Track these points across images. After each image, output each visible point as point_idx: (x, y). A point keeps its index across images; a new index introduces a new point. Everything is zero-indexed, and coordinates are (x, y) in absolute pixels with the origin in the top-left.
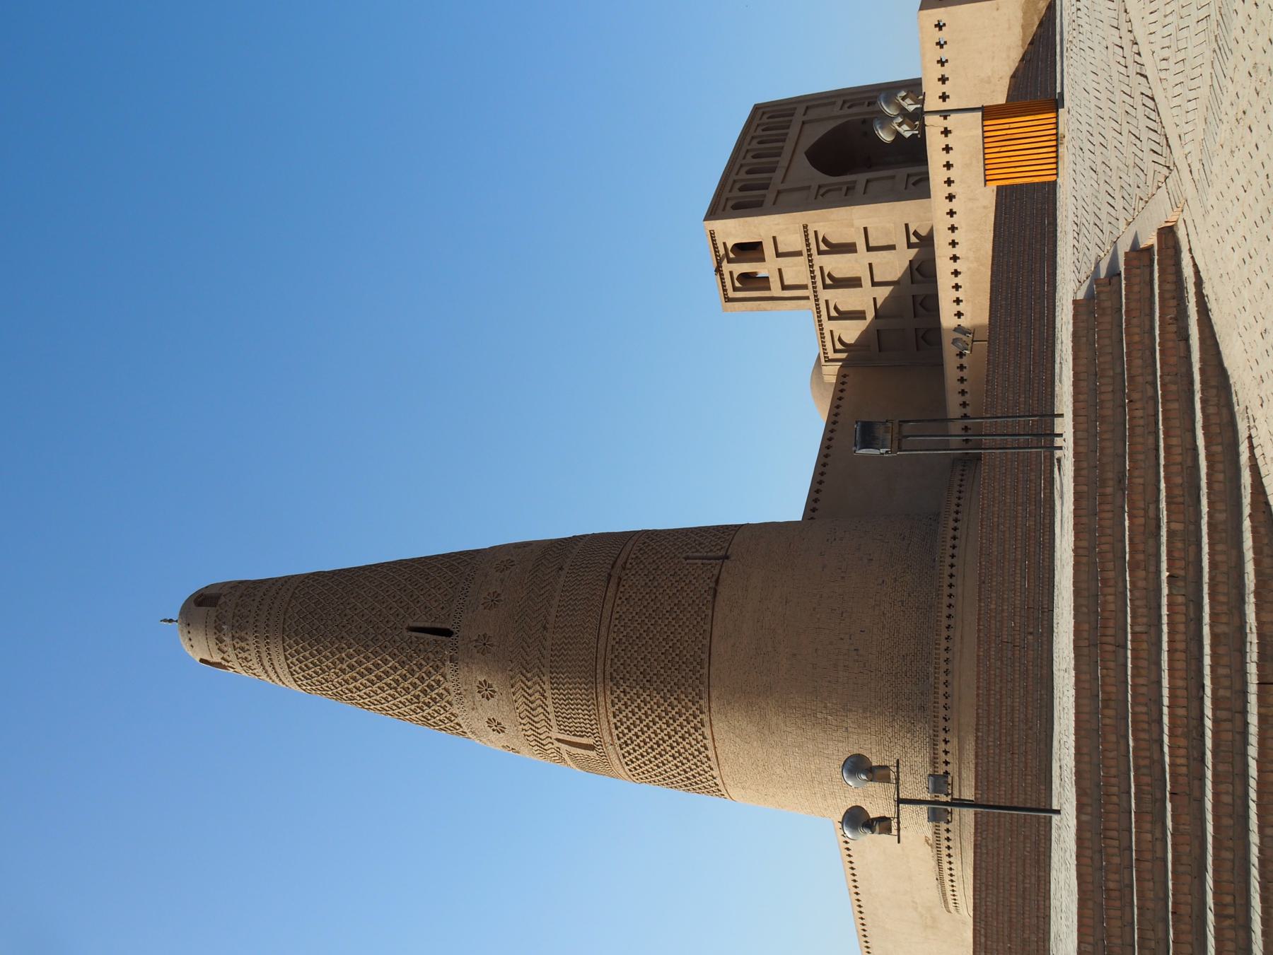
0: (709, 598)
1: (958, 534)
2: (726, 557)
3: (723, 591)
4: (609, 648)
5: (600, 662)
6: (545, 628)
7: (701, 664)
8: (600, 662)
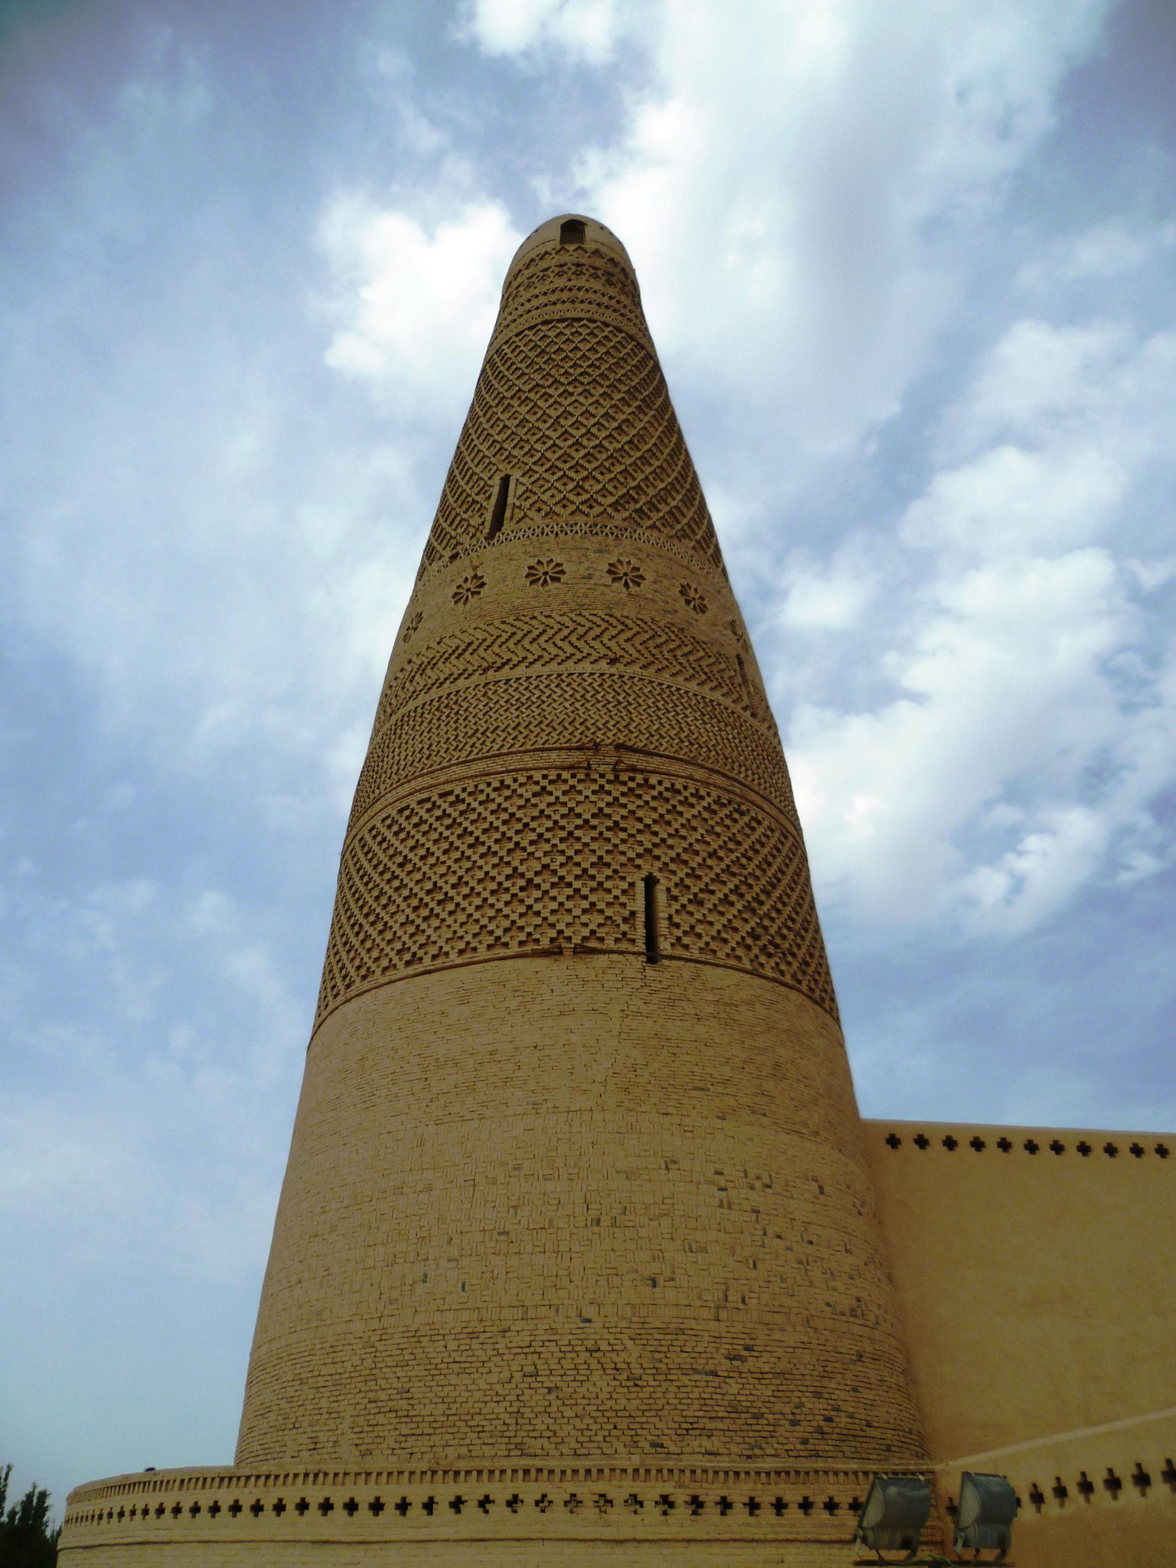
2: (652, 955)
4: (448, 788)
6: (485, 671)
7: (415, 960)
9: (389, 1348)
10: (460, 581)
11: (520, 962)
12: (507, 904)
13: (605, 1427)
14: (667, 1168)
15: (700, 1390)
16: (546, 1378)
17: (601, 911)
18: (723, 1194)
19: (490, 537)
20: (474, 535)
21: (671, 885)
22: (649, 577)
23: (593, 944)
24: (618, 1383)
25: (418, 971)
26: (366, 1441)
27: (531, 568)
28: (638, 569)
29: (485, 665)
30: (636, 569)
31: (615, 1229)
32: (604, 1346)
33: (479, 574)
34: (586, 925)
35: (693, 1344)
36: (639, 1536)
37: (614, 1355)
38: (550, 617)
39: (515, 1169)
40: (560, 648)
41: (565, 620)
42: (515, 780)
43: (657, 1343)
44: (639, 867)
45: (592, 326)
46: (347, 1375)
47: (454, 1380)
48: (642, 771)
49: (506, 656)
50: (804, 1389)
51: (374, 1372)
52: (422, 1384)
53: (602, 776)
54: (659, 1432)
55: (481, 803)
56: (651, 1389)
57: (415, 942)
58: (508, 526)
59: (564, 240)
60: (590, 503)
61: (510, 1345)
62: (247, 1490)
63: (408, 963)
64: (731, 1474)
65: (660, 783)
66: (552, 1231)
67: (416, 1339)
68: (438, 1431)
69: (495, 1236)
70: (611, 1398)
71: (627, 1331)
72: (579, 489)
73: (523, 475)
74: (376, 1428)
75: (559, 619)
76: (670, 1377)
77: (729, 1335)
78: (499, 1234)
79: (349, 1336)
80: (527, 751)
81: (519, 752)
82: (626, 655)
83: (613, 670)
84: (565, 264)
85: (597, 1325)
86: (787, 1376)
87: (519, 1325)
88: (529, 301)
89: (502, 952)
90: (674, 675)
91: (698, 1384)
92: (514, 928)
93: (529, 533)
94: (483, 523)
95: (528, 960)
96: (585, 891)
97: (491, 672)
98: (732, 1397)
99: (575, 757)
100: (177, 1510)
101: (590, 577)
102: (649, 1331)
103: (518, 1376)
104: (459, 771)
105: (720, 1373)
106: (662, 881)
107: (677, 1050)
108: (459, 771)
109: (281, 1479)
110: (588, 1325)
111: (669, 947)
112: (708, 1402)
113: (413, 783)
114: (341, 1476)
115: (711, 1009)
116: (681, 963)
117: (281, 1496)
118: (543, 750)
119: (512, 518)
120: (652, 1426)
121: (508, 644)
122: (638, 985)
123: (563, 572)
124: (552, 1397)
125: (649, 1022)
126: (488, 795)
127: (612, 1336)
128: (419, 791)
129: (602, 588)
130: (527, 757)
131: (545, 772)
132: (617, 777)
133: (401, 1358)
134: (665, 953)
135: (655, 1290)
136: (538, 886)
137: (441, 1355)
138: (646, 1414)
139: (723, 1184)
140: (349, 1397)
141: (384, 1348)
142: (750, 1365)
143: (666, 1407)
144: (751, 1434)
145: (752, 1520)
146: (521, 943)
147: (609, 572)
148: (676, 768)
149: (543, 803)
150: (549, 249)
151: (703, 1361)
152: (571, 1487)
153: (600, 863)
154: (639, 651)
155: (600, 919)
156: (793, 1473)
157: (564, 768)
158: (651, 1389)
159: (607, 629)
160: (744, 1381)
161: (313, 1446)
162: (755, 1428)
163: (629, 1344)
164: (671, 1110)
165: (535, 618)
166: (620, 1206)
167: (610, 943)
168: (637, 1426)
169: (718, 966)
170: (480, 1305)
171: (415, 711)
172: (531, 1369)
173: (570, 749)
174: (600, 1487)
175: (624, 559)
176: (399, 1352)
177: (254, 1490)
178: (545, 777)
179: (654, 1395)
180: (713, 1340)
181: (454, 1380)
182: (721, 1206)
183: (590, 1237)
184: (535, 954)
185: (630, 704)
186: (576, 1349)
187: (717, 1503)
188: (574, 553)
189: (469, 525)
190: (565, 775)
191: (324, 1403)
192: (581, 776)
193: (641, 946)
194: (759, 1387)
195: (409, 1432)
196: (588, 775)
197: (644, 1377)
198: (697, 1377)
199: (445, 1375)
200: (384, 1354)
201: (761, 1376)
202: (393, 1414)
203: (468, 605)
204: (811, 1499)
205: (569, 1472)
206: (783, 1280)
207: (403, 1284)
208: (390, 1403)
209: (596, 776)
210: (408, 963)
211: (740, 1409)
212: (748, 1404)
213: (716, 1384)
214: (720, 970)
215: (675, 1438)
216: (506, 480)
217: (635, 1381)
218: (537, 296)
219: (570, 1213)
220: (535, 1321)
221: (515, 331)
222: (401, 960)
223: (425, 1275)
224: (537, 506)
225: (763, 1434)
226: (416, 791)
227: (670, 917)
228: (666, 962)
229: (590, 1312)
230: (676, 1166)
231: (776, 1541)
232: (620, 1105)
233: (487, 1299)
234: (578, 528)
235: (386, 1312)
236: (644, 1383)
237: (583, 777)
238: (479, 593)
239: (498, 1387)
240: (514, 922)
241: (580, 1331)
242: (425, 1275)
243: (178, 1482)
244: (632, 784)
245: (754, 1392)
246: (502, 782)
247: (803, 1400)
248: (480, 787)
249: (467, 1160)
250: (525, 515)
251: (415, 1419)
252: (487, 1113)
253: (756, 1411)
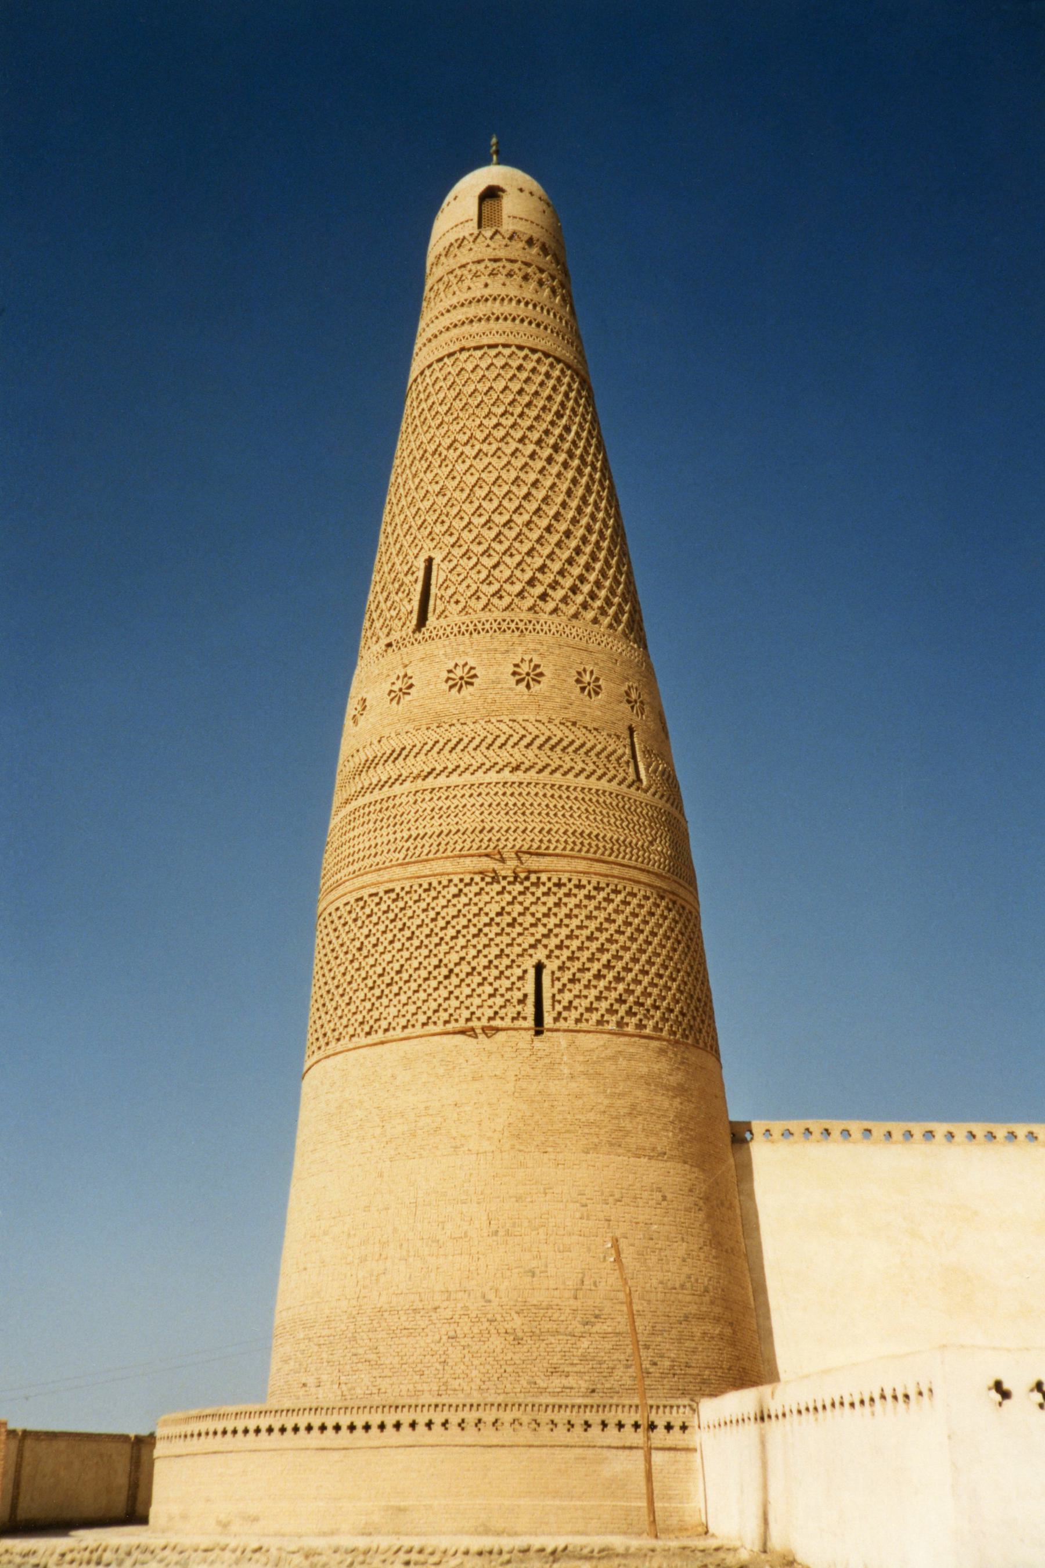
1: (596, 1430)
4: (390, 886)
18: (584, 1209)
30: (537, 666)
32: (499, 1318)
42: (440, 883)
48: (535, 872)
58: (432, 620)
65: (549, 879)
80: (448, 857)
81: (442, 858)
85: (495, 1304)
87: (446, 1304)
95: (451, 1036)
100: (235, 1432)
103: (445, 1338)
104: (398, 872)
115: (581, 1068)
118: (460, 856)
122: (529, 1053)
123: (475, 676)
124: (466, 1351)
125: (535, 1083)
128: (369, 886)
131: (462, 876)
139: (584, 1201)
142: (597, 1328)
157: (475, 873)
163: (515, 1316)
175: (527, 658)
178: (461, 880)
181: (404, 1340)
191: (325, 1356)
193: (530, 1023)
201: (604, 1335)
207: (371, 1275)
211: (589, 1358)
217: (518, 1340)
227: (554, 996)
228: (549, 1034)
229: (491, 1296)
232: (513, 1147)
239: (433, 1345)
246: (430, 884)
252: (424, 1153)
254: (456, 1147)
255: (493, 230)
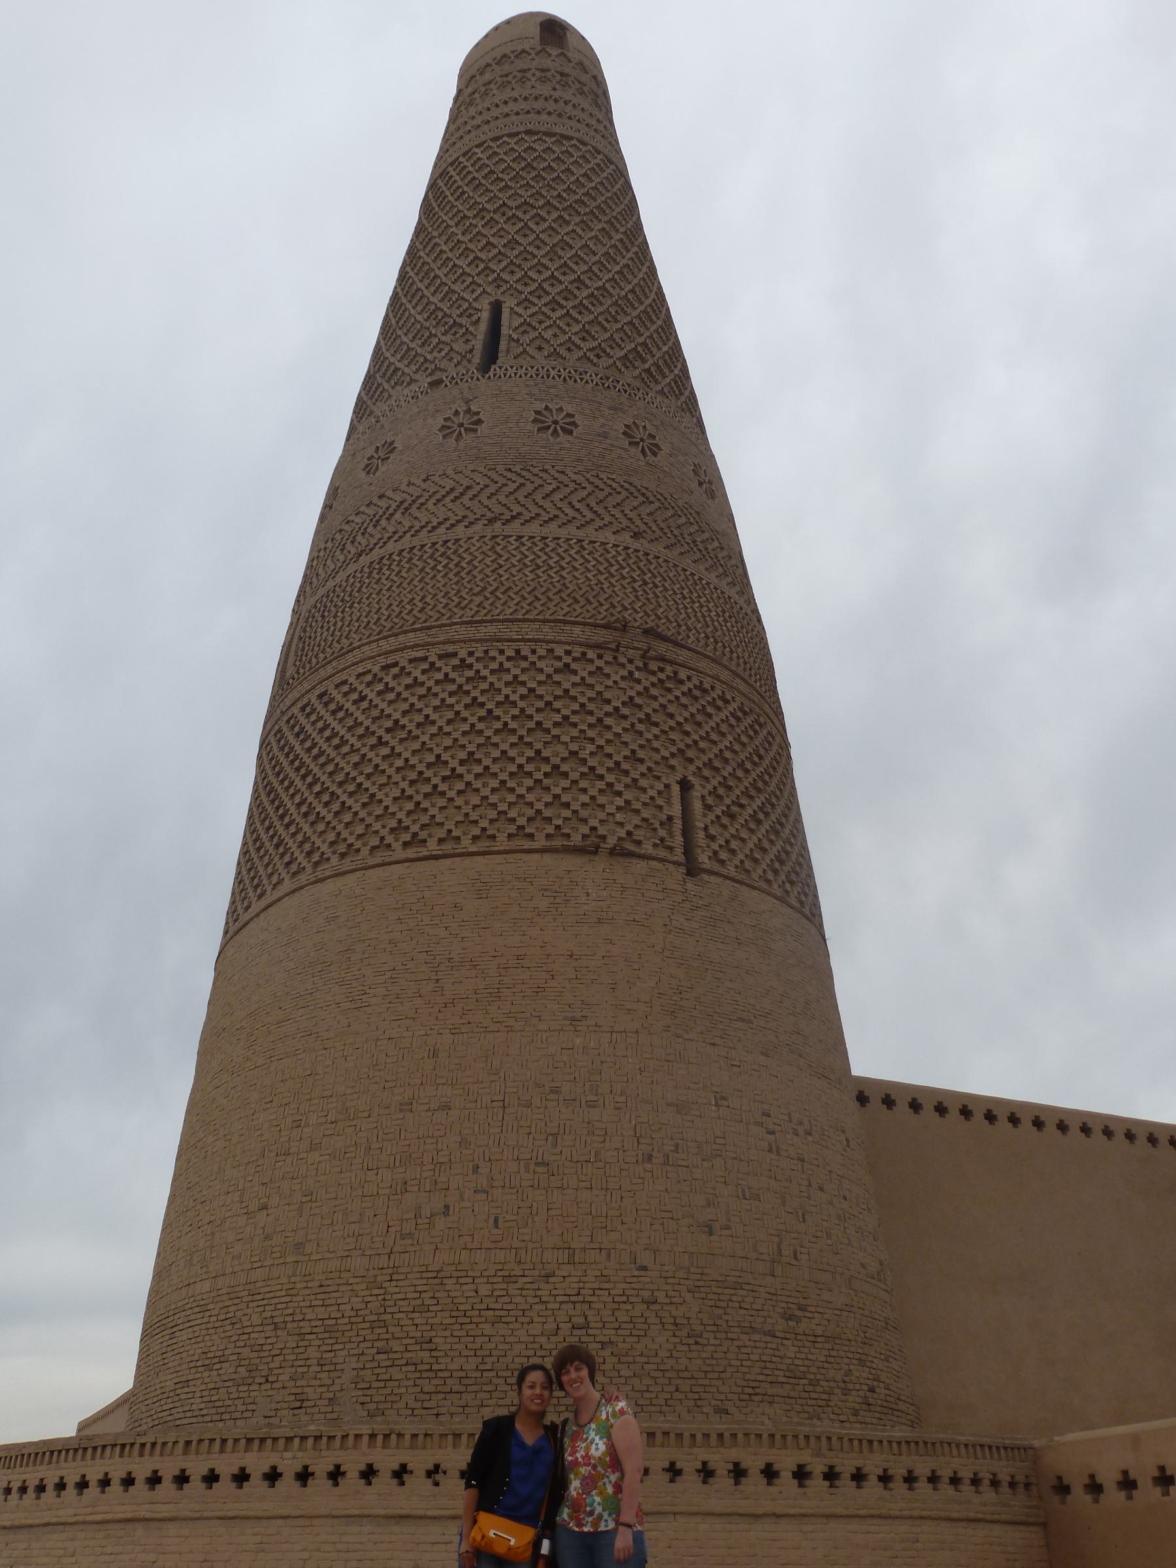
0: (576, 839)
1: (755, 1482)
2: (692, 870)
3: (592, 874)
4: (450, 648)
5: (422, 637)
6: (491, 521)
7: (415, 841)
8: (422, 637)
9: (403, 1290)
10: (449, 413)
11: (548, 859)
12: (529, 789)
13: (666, 1389)
14: (717, 1105)
15: (759, 1351)
16: (597, 1332)
17: (637, 811)
18: (772, 1137)
19: (485, 368)
20: (459, 363)
21: (706, 792)
22: (666, 448)
23: (631, 847)
24: (678, 1340)
25: (421, 855)
26: (375, 1399)
27: (537, 412)
28: (654, 437)
29: (489, 515)
30: (652, 437)
31: (669, 1168)
33: (474, 408)
34: (621, 824)
35: (752, 1300)
36: (778, 1511)
37: (672, 1308)
38: (563, 472)
39: (552, 1091)
40: (578, 510)
41: (579, 478)
42: (534, 652)
43: (716, 1297)
44: (672, 768)
45: (584, 149)
46: (346, 1320)
47: (488, 1329)
48: (671, 662)
49: (517, 509)
50: (851, 1355)
51: (383, 1317)
52: (447, 1333)
53: (631, 661)
54: (722, 1397)
55: (493, 672)
56: (713, 1348)
57: (414, 821)
59: (543, 41)
60: (599, 352)
61: (554, 1292)
62: (288, 1455)
63: (406, 845)
64: (865, 1443)
65: (689, 678)
66: (601, 1165)
67: (438, 1281)
68: (470, 1388)
69: (532, 1166)
70: (672, 1356)
71: (686, 1282)
72: (585, 334)
73: (518, 305)
74: (389, 1384)
75: (574, 477)
76: (730, 1336)
77: (786, 1293)
78: (537, 1164)
79: (345, 1275)
82: (561, 515)
83: (637, 545)
84: (548, 70)
86: (837, 1341)
88: (506, 103)
89: (527, 844)
90: (695, 562)
91: (758, 1344)
92: (539, 817)
93: (533, 372)
94: (471, 351)
95: (555, 856)
96: (619, 787)
97: (498, 524)
98: (790, 1361)
99: (601, 636)
101: (605, 436)
102: (708, 1284)
104: (463, 632)
105: (777, 1334)
106: (697, 787)
107: (720, 975)
108: (463, 632)
109: (338, 1441)
110: (643, 1273)
111: (706, 860)
112: (768, 1365)
113: (401, 638)
114: (421, 1437)
116: (719, 880)
117: (339, 1461)
118: (565, 622)
119: (508, 351)
120: (715, 1390)
121: (516, 495)
122: (679, 898)
126: (501, 664)
127: (669, 1287)
128: (412, 647)
129: (619, 451)
130: (546, 628)
131: (568, 648)
132: (645, 665)
133: (419, 1302)
134: (704, 866)
135: (712, 1238)
136: (565, 775)
137: (471, 1300)
138: (710, 1376)
139: (771, 1127)
140: (348, 1346)
141: (397, 1290)
143: (729, 1369)
144: (810, 1402)
145: (887, 1493)
146: (548, 836)
147: (624, 433)
148: (703, 664)
149: (567, 681)
150: (527, 48)
151: (761, 1320)
152: (702, 1454)
153: (633, 757)
154: (662, 529)
155: (636, 820)
156: (921, 1443)
158: (713, 1348)
159: (558, 488)
160: (800, 1344)
161: (298, 1404)
162: (813, 1395)
163: (688, 1296)
164: (717, 1041)
165: (546, 471)
166: (672, 1142)
167: (647, 848)
168: (701, 1389)
169: (754, 888)
170: (516, 1244)
171: (399, 554)
172: (581, 1320)
173: (596, 626)
174: (734, 1454)
176: (418, 1295)
177: (300, 1454)
179: (715, 1356)
180: (770, 1296)
181: (488, 1329)
182: (770, 1151)
183: (642, 1175)
184: (567, 850)
185: (563, 568)
186: (632, 1299)
187: (698, 1471)
188: (585, 404)
189: (452, 349)
190: (591, 654)
191: (313, 1353)
192: (608, 657)
194: (813, 1350)
195: (433, 1389)
196: (615, 658)
197: (706, 1335)
198: (756, 1337)
199: (477, 1324)
200: (395, 1297)
202: (412, 1368)
203: (462, 444)
204: (939, 1473)
205: (699, 1436)
206: (829, 1236)
208: (407, 1355)
209: (624, 661)
210: (406, 845)
212: (805, 1369)
213: (774, 1346)
214: (755, 893)
215: (738, 1403)
216: (496, 308)
218: (516, 100)
219: (619, 1146)
220: (584, 1267)
221: (492, 135)
222: (397, 840)
223: (447, 1207)
224: (537, 343)
225: (820, 1403)
226: (406, 648)
227: (706, 828)
228: (705, 876)
229: (646, 1259)
230: (725, 1103)
231: (911, 1517)
232: (667, 1029)
233: (526, 1238)
234: (586, 377)
235: (397, 1249)
236: (705, 1342)
237: (610, 659)
238: (476, 430)
240: (539, 812)
241: (635, 1279)
242: (447, 1207)
243: (181, 1444)
244: (662, 676)
245: (810, 1357)
246: (518, 652)
247: (852, 1367)
248: (491, 654)
249: (494, 1078)
250: (525, 351)
251: (440, 1374)
253: (812, 1377)
254: (573, 1019)
255: (560, 51)
